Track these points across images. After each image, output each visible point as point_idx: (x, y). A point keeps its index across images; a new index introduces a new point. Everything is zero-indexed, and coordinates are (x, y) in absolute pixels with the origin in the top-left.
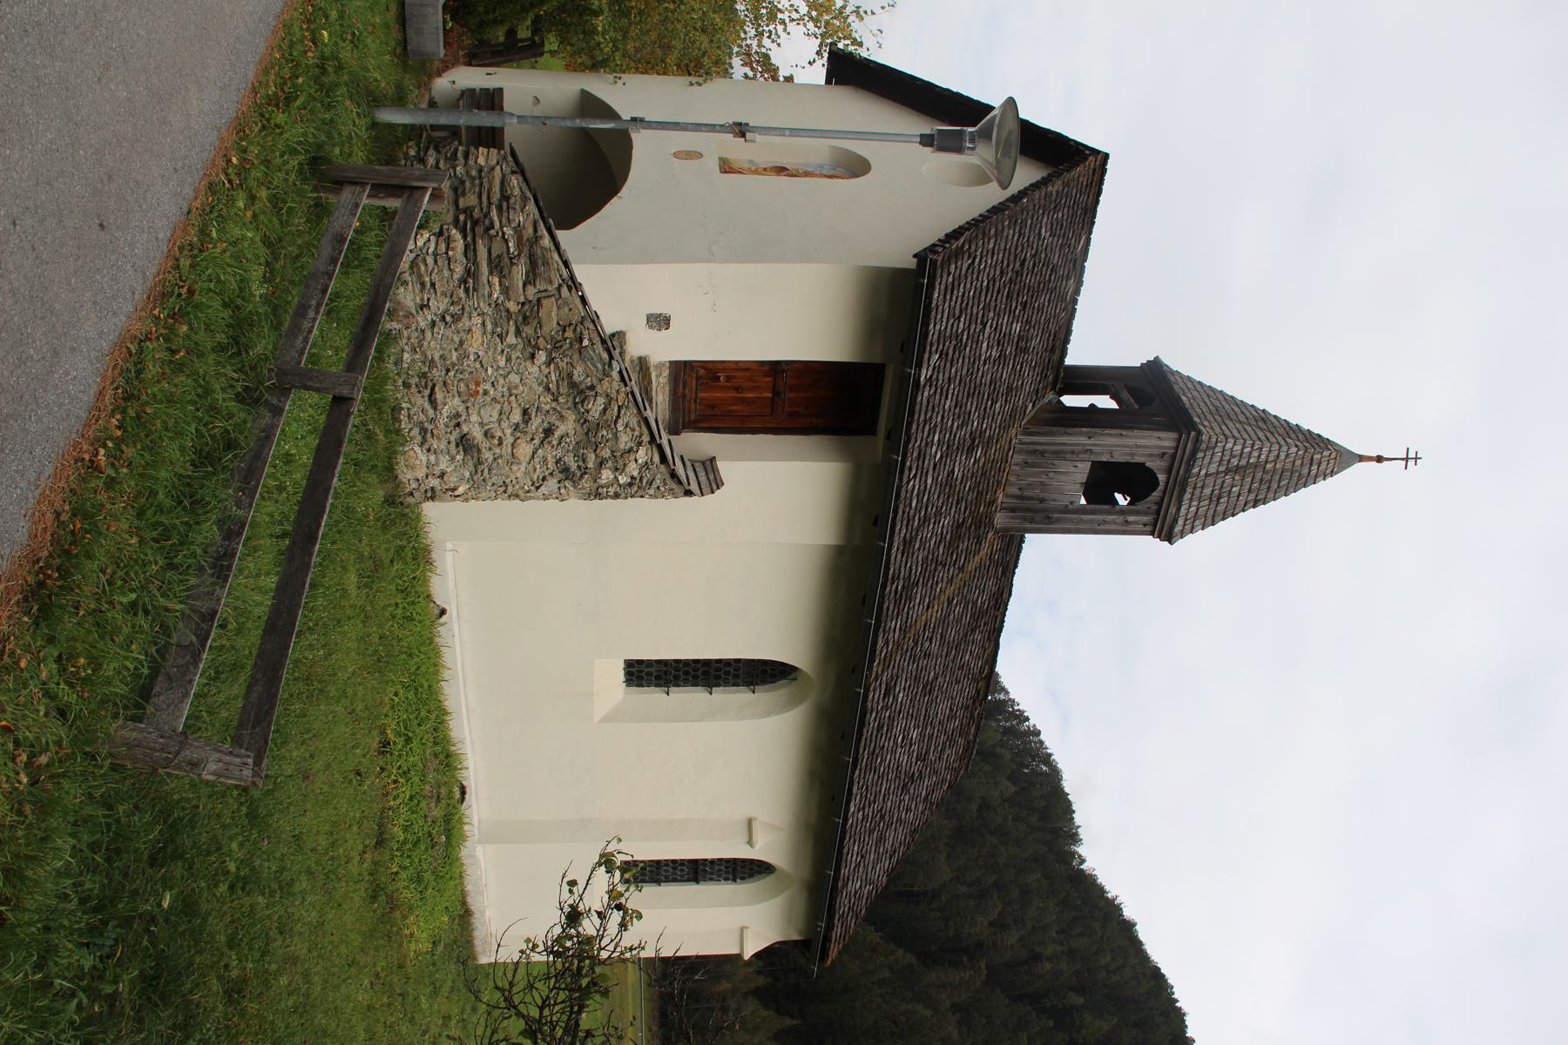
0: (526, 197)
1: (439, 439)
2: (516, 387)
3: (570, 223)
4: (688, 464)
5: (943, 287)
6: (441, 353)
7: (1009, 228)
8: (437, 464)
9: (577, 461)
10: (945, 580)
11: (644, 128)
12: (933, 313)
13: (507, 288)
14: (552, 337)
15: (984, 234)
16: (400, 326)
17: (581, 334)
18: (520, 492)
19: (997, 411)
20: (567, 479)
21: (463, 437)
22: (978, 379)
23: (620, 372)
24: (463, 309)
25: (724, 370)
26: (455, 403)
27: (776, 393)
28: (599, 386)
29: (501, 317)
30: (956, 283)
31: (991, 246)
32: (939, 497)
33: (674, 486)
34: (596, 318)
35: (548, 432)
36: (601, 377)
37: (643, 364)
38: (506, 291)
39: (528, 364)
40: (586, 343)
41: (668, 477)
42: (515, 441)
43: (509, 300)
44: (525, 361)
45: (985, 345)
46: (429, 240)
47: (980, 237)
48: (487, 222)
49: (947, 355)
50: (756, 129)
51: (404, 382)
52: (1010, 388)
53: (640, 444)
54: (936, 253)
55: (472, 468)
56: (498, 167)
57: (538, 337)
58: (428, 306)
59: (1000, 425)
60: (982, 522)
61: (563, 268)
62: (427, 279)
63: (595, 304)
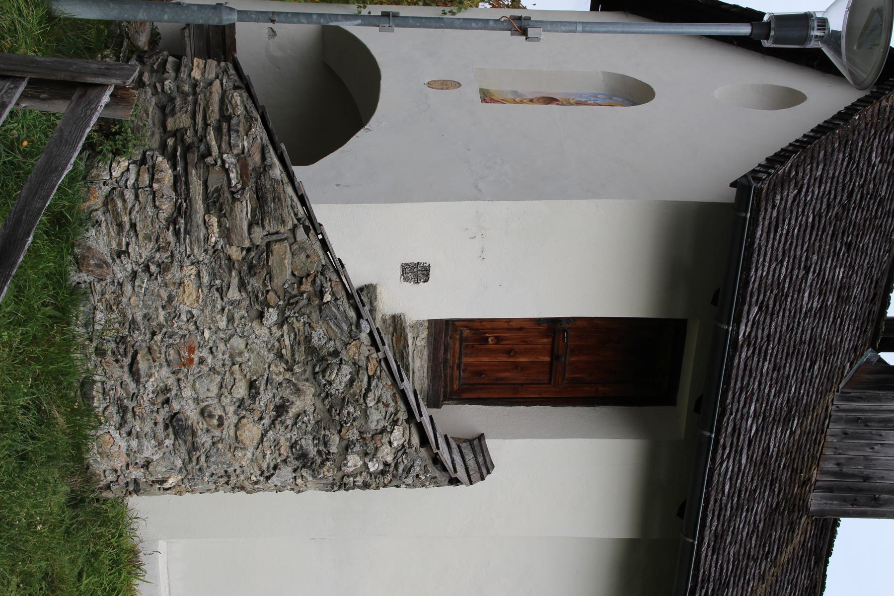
0: (251, 117)
1: (142, 419)
2: (240, 354)
3: (309, 159)
4: (454, 445)
5: (767, 223)
6: (145, 311)
7: (839, 151)
8: (140, 451)
9: (317, 445)
10: (757, 578)
11: (398, 26)
12: (755, 256)
13: (228, 229)
14: (286, 291)
15: (812, 158)
16: (91, 278)
17: (322, 286)
18: (247, 484)
19: (816, 373)
20: (304, 466)
21: (174, 416)
22: (799, 335)
23: (371, 334)
24: (172, 256)
25: (493, 330)
26: (162, 375)
27: (555, 356)
28: (344, 352)
29: (220, 267)
30: (781, 217)
31: (819, 173)
32: (752, 479)
33: (437, 473)
34: (340, 268)
35: (281, 409)
36: (347, 340)
37: (397, 323)
38: (227, 234)
39: (255, 324)
40: (327, 298)
41: (429, 462)
42: (240, 420)
43: (231, 245)
44: (252, 321)
45: (807, 294)
46: (128, 170)
47: (808, 161)
48: (202, 147)
49: (767, 307)
50: (539, 24)
51: (96, 349)
52: (829, 346)
53: (395, 423)
54: (759, 180)
55: (184, 454)
56: (218, 81)
57: (268, 291)
58: (127, 253)
59: (818, 389)
60: (799, 506)
61: (299, 205)
62: (126, 219)
63: (339, 250)
